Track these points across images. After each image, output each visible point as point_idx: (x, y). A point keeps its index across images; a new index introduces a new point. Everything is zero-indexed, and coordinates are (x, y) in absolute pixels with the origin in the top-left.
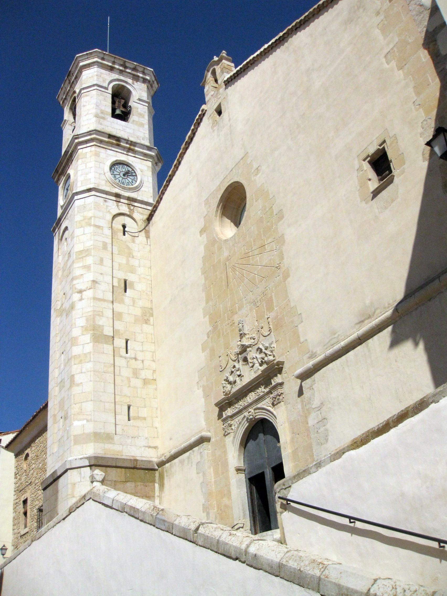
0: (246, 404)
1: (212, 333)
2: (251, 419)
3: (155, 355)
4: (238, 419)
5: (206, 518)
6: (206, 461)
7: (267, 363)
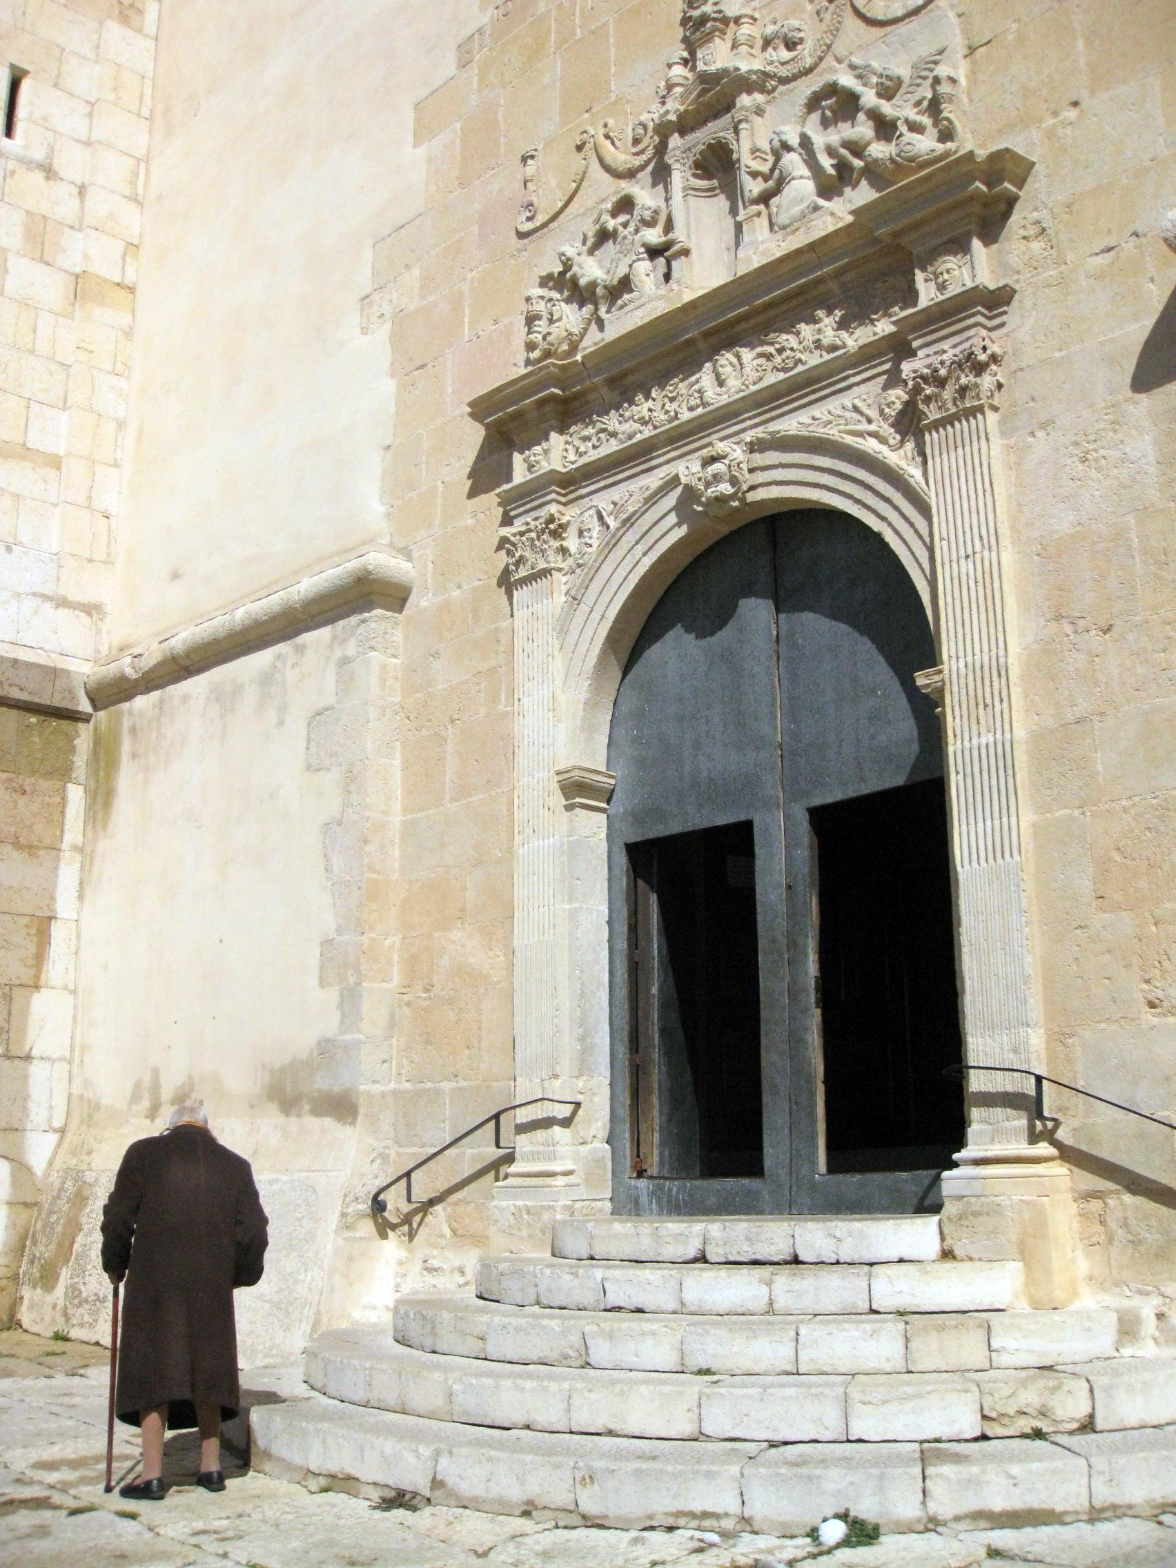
0: (686, 416)
1: (488, 40)
2: (721, 500)
3: (147, 171)
4: (616, 498)
5: (335, 1017)
6: (373, 714)
7: (874, 173)
